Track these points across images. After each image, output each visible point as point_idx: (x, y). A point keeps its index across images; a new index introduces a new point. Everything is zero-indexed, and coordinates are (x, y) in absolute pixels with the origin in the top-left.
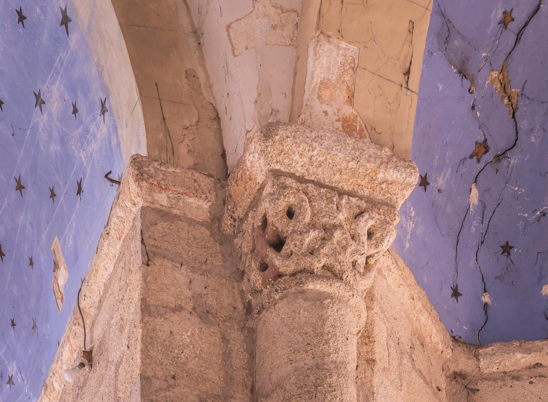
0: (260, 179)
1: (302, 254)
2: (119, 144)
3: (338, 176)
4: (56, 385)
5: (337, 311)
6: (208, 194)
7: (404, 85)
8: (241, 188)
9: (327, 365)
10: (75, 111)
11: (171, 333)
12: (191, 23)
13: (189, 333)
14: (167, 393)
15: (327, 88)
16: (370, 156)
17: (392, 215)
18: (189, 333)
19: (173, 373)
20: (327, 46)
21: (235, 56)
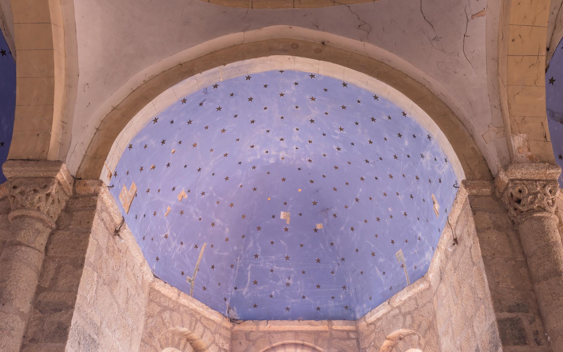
0: (507, 182)
1: (529, 204)
2: (454, 171)
3: (533, 176)
4: (442, 247)
5: (548, 222)
6: (489, 187)
7: (546, 141)
8: (500, 184)
9: (550, 243)
10: (435, 160)
11: (489, 237)
12: (469, 133)
13: (495, 236)
14: (493, 261)
15: (520, 149)
16: (542, 167)
17: (556, 184)
18: (495, 236)
19: (493, 253)
20: (517, 137)
21: (487, 143)
